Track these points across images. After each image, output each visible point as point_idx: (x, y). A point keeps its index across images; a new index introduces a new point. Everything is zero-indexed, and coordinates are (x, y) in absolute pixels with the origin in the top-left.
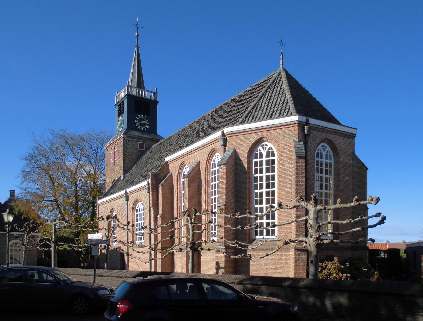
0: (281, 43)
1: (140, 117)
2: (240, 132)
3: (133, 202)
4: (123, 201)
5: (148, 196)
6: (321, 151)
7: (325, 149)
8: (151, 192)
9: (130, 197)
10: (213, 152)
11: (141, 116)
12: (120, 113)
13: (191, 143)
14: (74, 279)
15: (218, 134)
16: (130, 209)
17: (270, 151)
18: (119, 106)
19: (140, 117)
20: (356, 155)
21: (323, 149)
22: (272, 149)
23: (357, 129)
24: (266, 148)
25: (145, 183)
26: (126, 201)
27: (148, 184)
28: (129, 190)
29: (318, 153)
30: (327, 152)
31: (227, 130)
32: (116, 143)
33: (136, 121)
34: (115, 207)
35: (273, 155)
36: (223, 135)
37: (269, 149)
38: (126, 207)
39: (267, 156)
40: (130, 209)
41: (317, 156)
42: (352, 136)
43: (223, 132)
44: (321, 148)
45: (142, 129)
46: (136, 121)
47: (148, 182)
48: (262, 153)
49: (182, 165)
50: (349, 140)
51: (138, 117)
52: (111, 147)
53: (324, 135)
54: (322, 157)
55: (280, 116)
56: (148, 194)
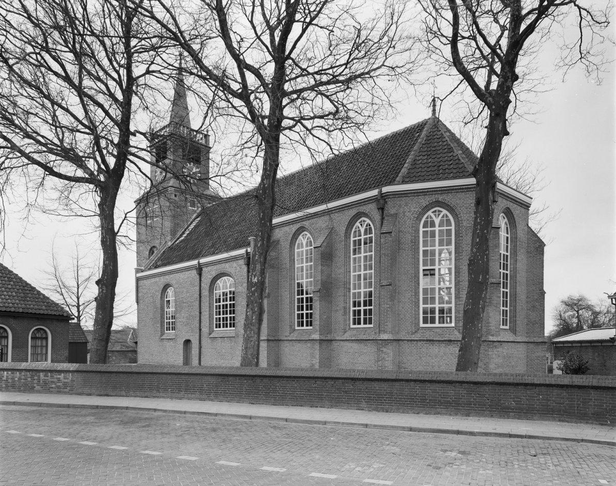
21: (435, 215)
25: (242, 251)
37: (443, 217)
43: (381, 191)
44: (432, 215)
53: (424, 201)
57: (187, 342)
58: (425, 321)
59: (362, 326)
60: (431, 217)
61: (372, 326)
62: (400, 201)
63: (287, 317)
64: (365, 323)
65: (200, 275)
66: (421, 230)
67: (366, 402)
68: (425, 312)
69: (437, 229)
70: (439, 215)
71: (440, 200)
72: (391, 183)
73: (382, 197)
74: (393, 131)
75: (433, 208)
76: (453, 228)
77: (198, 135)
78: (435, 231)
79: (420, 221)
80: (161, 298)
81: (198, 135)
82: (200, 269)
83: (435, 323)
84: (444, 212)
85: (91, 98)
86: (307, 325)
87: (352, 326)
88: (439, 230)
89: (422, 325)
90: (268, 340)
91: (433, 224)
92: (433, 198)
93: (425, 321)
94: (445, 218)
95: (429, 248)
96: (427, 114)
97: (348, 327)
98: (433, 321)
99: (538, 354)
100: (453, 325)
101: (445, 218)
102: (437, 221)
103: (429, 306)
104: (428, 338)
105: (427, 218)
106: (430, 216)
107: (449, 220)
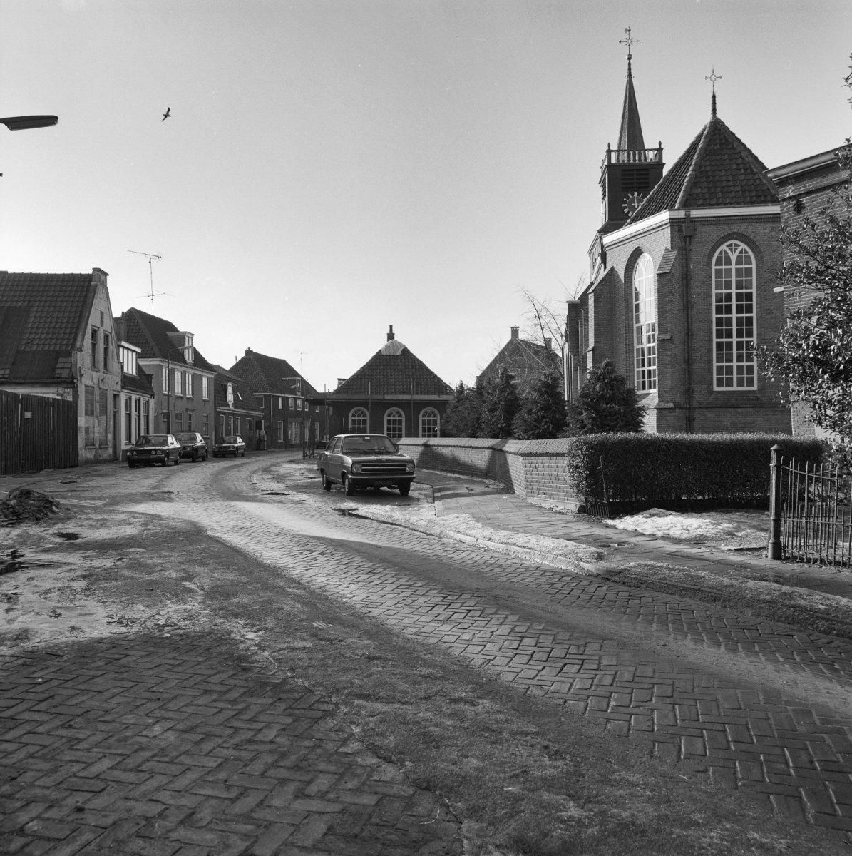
21: (731, 250)
37: (741, 252)
39: (739, 262)
51: (628, 198)
53: (724, 230)
58: (720, 383)
60: (726, 253)
63: (35, 391)
66: (714, 268)
68: (719, 300)
69: (734, 267)
70: (736, 250)
75: (728, 240)
76: (754, 266)
77: (563, 685)
78: (731, 318)
81: (563, 685)
84: (743, 246)
85: (38, 704)
86: (740, 383)
88: (738, 367)
91: (728, 262)
93: (720, 383)
95: (725, 364)
101: (744, 255)
102: (733, 258)
103: (724, 291)
105: (721, 253)
107: (749, 257)
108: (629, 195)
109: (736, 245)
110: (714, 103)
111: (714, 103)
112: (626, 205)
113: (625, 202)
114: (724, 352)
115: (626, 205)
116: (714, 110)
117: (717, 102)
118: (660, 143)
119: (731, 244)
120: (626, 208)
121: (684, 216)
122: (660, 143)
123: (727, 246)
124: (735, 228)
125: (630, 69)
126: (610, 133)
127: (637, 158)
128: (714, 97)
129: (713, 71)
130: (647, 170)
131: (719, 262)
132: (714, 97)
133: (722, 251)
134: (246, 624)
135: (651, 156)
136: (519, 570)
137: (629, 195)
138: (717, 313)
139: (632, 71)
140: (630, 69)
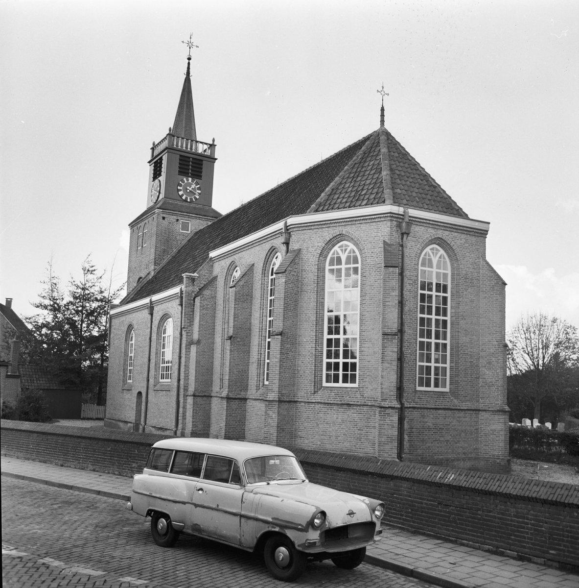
0: (382, 91)
1: (186, 181)
2: (17, 372)
3: (159, 318)
4: (146, 313)
5: (180, 310)
6: (429, 255)
7: (437, 254)
8: (184, 305)
9: (155, 308)
10: (272, 251)
11: (188, 180)
12: (156, 174)
13: (247, 233)
14: (312, 552)
15: (279, 225)
16: (155, 329)
17: (352, 254)
18: (155, 163)
19: (186, 181)
20: (487, 263)
21: (433, 253)
22: (354, 252)
23: (489, 223)
24: (346, 250)
25: (176, 290)
26: (149, 316)
27: (181, 291)
28: (155, 297)
29: (424, 259)
30: (440, 257)
31: (292, 220)
32: (146, 221)
33: (179, 188)
34: (134, 323)
35: (356, 261)
36: (286, 226)
37: (350, 252)
38: (149, 325)
40: (155, 329)
41: (423, 265)
42: (483, 233)
43: (286, 223)
44: (430, 252)
45: (189, 200)
46: (179, 188)
47: (181, 289)
48: (340, 257)
49: (232, 267)
50: (473, 239)
51: (183, 182)
52: (139, 226)
53: (432, 233)
54: (431, 266)
55: (370, 203)
56: (180, 308)
57: (140, 393)
59: (340, 384)
61: (356, 385)
62: (304, 234)
64: (345, 380)
65: (152, 314)
67: (92, 465)
71: (344, 233)
72: (302, 211)
73: (288, 230)
74: (349, 145)
79: (326, 257)
80: (126, 340)
82: (151, 308)
83: (338, 382)
86: (436, 385)
87: (325, 384)
89: (325, 384)
90: (228, 398)
92: (440, 233)
94: (427, 257)
96: (377, 126)
97: (261, 384)
98: (336, 380)
99: (493, 427)
100: (447, 390)
102: (344, 258)
104: (326, 401)
106: (429, 254)
108: (185, 179)
109: (437, 250)
110: (382, 115)
111: (382, 115)
112: (181, 188)
113: (181, 185)
114: (441, 353)
115: (181, 188)
116: (382, 121)
117: (385, 114)
118: (214, 140)
119: (434, 248)
120: (181, 190)
121: (402, 213)
122: (214, 140)
123: (431, 249)
124: (440, 233)
125: (188, 68)
126: (164, 121)
127: (189, 147)
128: (383, 110)
129: (383, 88)
130: (202, 161)
131: (332, 263)
132: (383, 110)
133: (334, 252)
134: (38, 436)
135: (201, 149)
136: (55, 483)
137: (185, 179)
138: (420, 313)
139: (190, 70)
140: (188, 68)
